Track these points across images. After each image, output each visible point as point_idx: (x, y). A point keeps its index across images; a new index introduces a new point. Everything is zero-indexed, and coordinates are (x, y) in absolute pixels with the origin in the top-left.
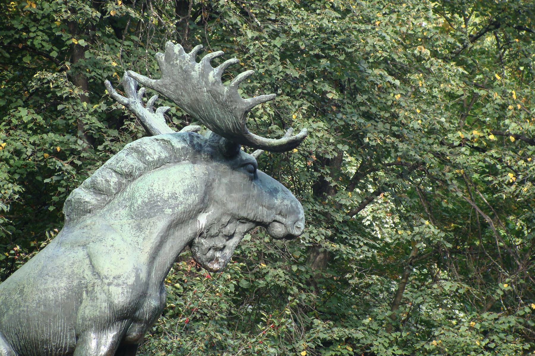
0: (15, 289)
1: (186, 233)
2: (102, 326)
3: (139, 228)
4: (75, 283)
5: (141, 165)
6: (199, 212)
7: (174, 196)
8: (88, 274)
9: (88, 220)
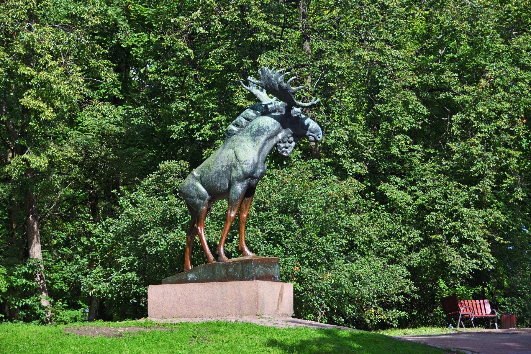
0: (206, 167)
1: (274, 141)
2: (240, 180)
3: (254, 141)
4: (229, 164)
5: (255, 115)
6: (278, 133)
7: (268, 127)
8: (234, 159)
9: (234, 137)
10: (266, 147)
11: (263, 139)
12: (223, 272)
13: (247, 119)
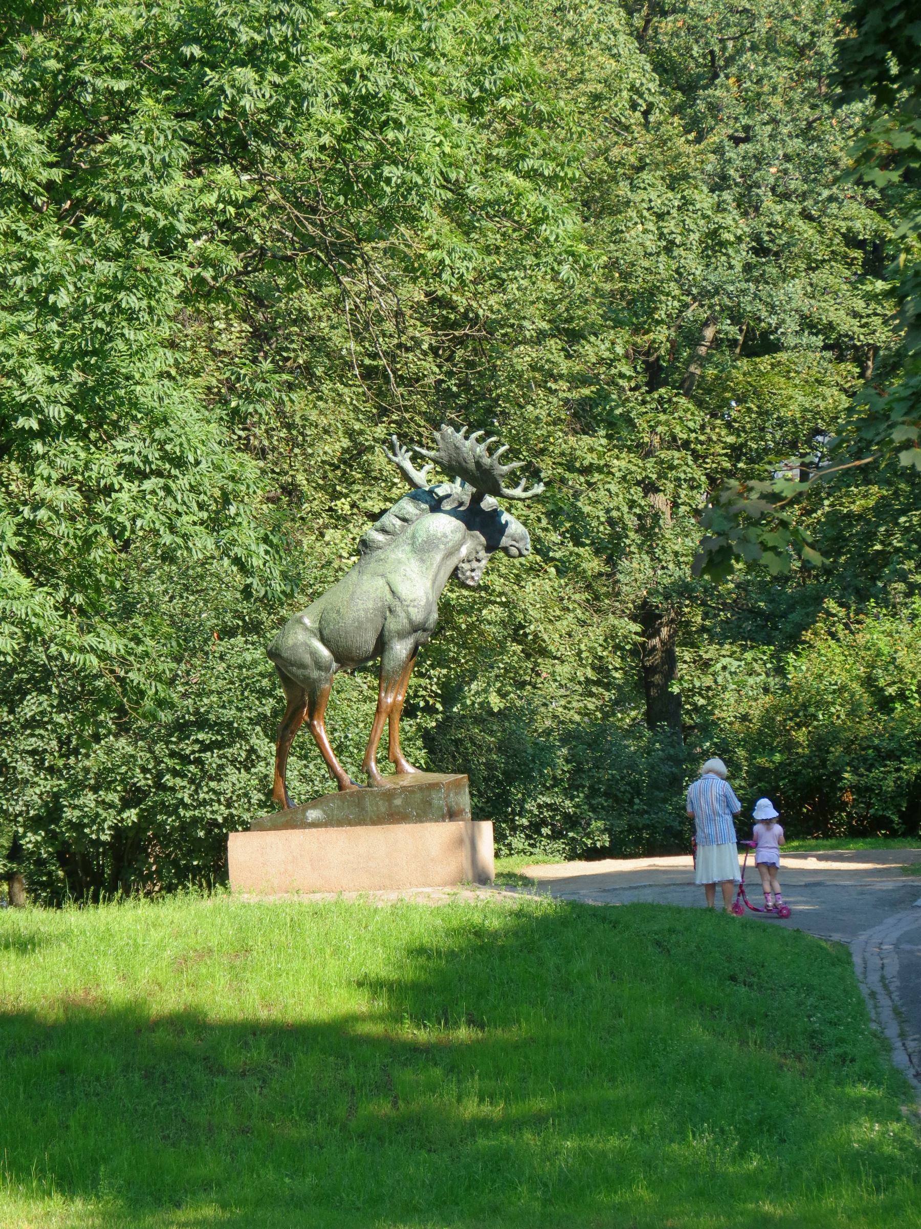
2: (402, 635)
3: (422, 561)
8: (389, 596)
10: (442, 573)
11: (438, 557)
12: (383, 807)
13: (404, 520)
